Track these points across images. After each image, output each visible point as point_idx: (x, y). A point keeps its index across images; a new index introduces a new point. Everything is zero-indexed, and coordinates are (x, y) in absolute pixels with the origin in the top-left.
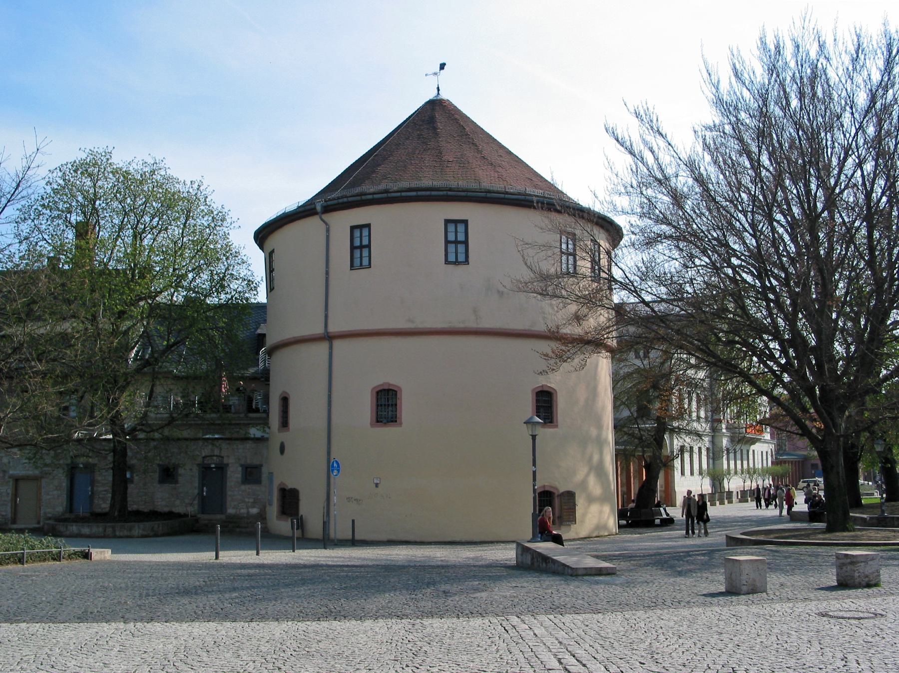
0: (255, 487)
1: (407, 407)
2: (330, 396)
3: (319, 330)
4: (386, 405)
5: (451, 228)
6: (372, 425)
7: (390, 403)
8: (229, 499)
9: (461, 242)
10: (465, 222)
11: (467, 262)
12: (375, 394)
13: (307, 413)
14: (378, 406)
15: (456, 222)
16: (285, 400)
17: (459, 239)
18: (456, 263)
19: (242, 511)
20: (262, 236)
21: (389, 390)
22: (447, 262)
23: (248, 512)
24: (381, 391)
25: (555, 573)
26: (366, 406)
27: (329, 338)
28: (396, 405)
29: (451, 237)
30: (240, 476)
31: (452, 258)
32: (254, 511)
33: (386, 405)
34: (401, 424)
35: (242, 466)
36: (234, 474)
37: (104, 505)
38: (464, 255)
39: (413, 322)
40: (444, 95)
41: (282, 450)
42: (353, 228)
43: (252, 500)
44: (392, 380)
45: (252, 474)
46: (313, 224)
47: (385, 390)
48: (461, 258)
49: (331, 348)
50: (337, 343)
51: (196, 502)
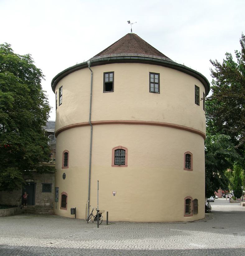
0: (49, 194)
1: (130, 159)
2: (91, 152)
3: (86, 120)
4: (120, 157)
5: (152, 76)
6: (184, 169)
7: (121, 155)
8: (36, 198)
9: (156, 83)
10: (158, 74)
11: (159, 92)
12: (114, 151)
13: (78, 159)
14: (115, 157)
15: (155, 74)
16: (66, 154)
17: (153, 84)
18: (154, 92)
19: (42, 204)
20: (56, 82)
21: (121, 150)
22: (150, 92)
23: (45, 205)
24: (117, 150)
25: (64, 219)
26: (109, 157)
27: (91, 124)
28: (125, 157)
29: (152, 80)
30: (42, 188)
31: (152, 90)
32: (48, 204)
33: (120, 157)
34: (184, 169)
35: (42, 184)
36: (39, 188)
37: (121, 150)
38: (158, 89)
39: (134, 118)
40: (134, 32)
41: (64, 176)
42: (105, 73)
43: (47, 199)
44: (123, 145)
45: (47, 188)
46: (84, 74)
47: (119, 149)
48: (157, 90)
49: (92, 129)
50: (95, 127)
51: (21, 200)
